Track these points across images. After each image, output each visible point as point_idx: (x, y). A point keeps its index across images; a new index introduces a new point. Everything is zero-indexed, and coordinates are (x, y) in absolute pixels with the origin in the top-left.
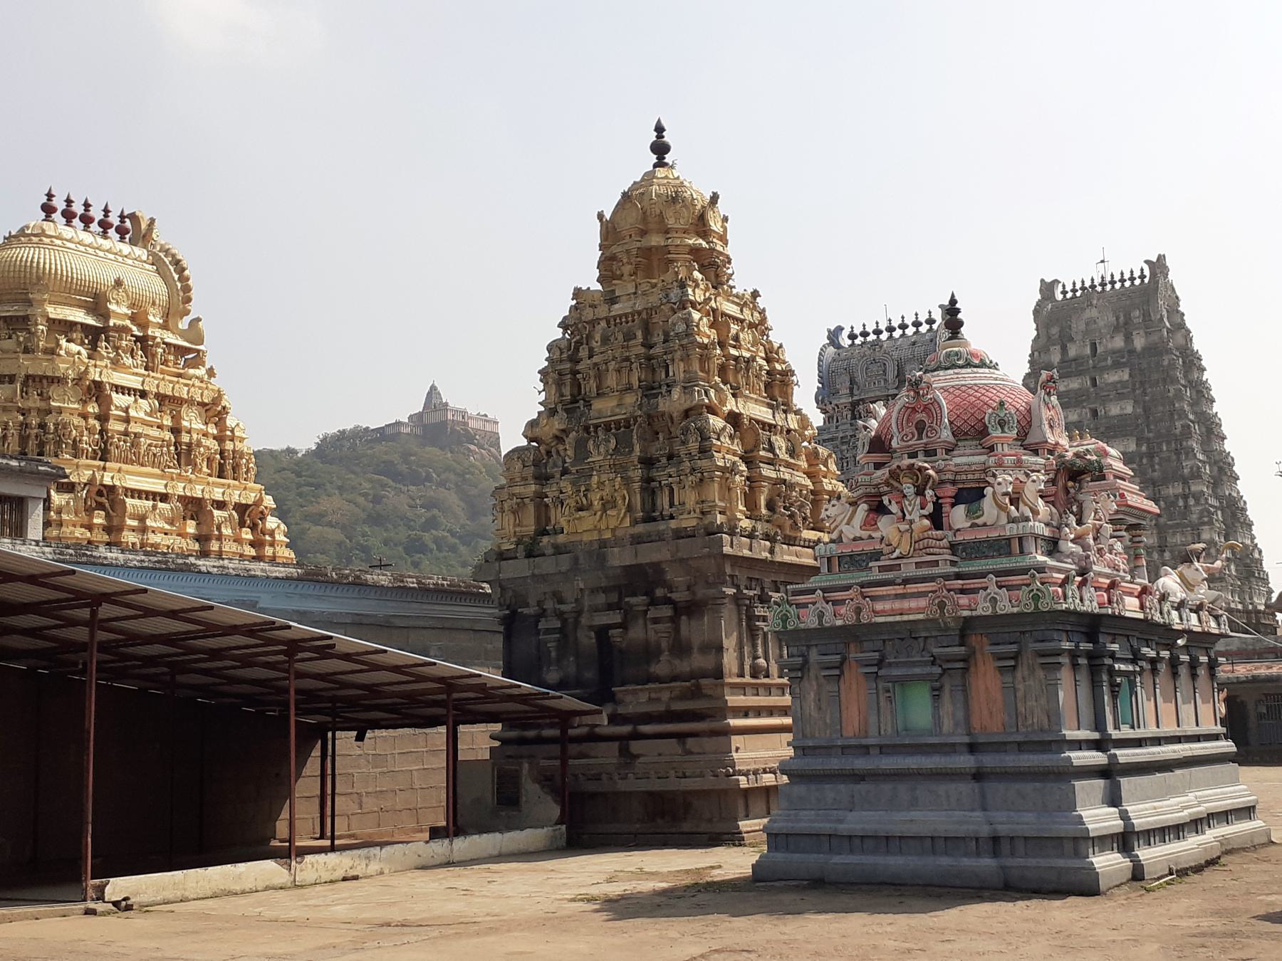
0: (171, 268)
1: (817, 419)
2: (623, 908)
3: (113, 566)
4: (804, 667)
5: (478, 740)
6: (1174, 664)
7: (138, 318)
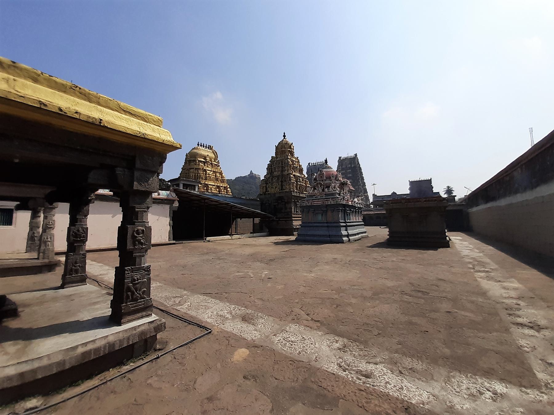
0: (215, 153)
1: (306, 176)
2: (277, 244)
3: (207, 195)
4: (303, 211)
5: (257, 220)
6: (356, 211)
7: (211, 160)
